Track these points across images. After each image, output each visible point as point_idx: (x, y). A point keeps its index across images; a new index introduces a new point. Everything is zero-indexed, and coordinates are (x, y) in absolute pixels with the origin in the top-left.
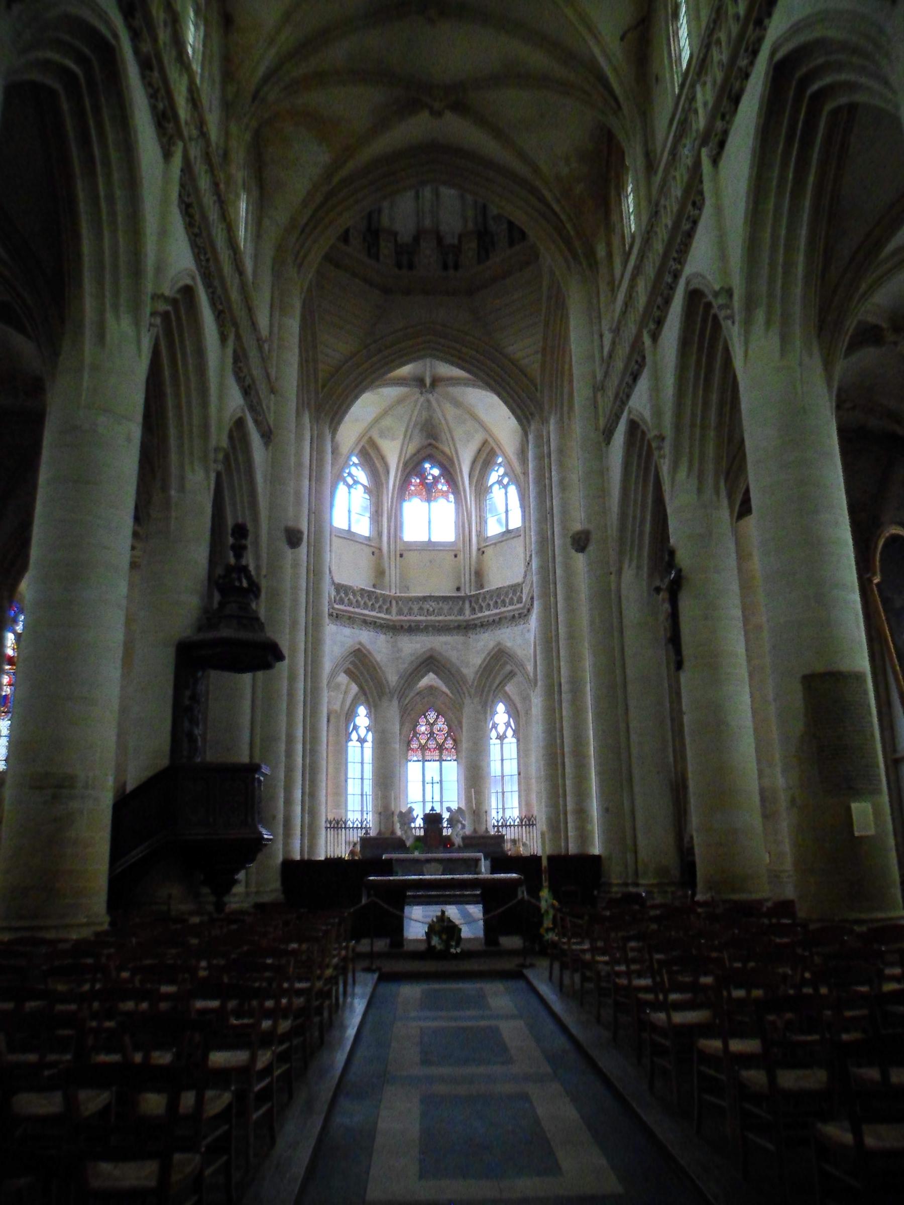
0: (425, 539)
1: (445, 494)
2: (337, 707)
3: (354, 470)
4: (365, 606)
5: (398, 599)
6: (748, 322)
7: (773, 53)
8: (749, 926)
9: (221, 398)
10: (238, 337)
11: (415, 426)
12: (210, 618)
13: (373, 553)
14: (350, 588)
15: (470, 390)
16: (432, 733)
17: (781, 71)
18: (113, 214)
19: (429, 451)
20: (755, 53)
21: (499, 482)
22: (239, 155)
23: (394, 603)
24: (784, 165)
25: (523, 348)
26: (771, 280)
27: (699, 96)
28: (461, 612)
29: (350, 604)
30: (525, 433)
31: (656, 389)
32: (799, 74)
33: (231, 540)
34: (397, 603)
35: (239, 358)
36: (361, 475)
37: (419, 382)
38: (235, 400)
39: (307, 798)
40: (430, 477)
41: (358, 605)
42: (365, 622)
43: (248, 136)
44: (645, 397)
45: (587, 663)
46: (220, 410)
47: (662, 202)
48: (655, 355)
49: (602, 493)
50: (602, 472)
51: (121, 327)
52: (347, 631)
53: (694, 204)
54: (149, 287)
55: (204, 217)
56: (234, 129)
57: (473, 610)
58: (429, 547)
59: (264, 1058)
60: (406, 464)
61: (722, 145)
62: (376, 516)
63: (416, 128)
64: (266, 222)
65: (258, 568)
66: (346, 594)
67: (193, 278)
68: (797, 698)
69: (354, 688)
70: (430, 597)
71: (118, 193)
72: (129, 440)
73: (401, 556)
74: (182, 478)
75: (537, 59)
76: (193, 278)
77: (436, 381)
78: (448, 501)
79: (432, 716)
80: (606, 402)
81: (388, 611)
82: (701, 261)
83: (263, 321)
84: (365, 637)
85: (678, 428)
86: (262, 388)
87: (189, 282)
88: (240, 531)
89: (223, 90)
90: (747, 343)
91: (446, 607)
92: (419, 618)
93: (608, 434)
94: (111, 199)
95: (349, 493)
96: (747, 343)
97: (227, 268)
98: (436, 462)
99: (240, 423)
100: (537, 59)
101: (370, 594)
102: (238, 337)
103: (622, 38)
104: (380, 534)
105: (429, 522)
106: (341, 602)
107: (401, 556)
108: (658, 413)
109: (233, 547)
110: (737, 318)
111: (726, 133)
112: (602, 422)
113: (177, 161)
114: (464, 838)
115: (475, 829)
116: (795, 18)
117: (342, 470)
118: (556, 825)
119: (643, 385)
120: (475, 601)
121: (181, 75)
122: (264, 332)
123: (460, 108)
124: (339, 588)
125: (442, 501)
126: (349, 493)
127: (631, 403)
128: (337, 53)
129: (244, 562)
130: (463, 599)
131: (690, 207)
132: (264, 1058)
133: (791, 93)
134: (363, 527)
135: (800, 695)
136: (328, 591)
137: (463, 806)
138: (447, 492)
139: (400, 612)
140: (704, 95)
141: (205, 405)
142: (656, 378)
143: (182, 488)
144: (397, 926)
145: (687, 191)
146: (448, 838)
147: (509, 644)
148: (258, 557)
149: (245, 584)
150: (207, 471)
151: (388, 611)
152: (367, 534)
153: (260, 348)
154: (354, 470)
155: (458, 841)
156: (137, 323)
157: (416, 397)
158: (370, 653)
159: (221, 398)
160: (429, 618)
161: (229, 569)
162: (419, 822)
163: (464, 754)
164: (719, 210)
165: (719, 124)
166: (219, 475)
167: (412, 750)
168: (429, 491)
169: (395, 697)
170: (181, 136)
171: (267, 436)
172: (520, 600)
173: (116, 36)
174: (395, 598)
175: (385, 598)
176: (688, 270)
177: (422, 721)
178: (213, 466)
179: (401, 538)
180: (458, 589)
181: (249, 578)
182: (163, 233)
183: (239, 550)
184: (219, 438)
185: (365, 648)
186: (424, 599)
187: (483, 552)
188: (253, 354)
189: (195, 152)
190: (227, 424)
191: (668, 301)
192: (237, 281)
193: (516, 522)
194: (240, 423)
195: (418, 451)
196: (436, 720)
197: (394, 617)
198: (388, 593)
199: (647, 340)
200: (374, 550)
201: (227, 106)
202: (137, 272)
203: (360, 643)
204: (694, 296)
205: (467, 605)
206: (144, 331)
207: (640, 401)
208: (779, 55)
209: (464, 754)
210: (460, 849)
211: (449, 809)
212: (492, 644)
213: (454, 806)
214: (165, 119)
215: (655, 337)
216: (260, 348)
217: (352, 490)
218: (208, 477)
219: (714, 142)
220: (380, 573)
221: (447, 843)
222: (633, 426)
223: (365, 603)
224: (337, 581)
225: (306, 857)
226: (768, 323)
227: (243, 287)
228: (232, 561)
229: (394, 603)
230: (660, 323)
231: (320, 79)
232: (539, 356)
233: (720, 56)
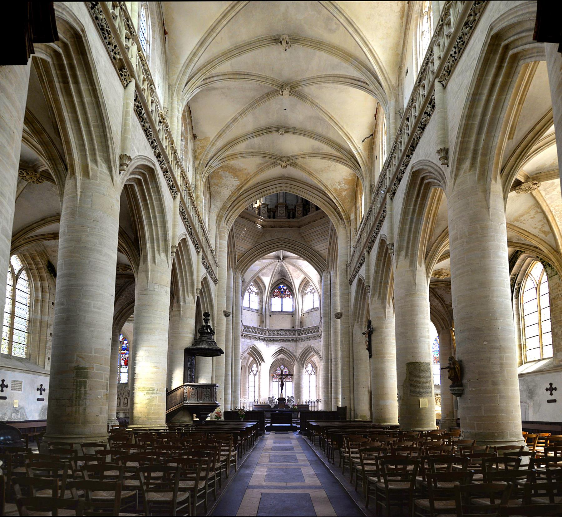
1: (289, 296)
2: (245, 364)
3: (251, 287)
5: (269, 331)
6: (398, 255)
7: (412, 168)
8: (375, 428)
9: (198, 272)
10: (203, 251)
11: (276, 272)
12: (196, 341)
15: (298, 260)
17: (415, 174)
18: (156, 222)
19: (282, 280)
20: (407, 166)
22: (201, 187)
24: (415, 205)
25: (321, 247)
26: (408, 242)
27: (387, 174)
28: (294, 335)
29: (250, 332)
30: (321, 277)
31: (368, 270)
32: (503, 44)
33: (203, 317)
35: (204, 258)
36: (255, 289)
37: (278, 258)
38: (203, 272)
43: (204, 180)
44: (364, 272)
45: (340, 353)
46: (198, 276)
47: (373, 207)
48: (369, 258)
49: (348, 301)
50: (348, 294)
51: (161, 258)
52: (249, 341)
53: (384, 211)
54: (170, 244)
55: (189, 215)
56: (198, 177)
57: (299, 334)
59: (202, 485)
60: (272, 285)
61: (394, 193)
63: (276, 171)
64: (213, 207)
65: (213, 324)
66: (248, 329)
67: (186, 235)
68: (405, 369)
69: (251, 359)
70: (282, 330)
71: (157, 215)
72: (166, 292)
74: (184, 299)
75: (327, 149)
76: (186, 235)
77: (284, 258)
80: (351, 271)
81: (265, 334)
82: (384, 230)
83: (212, 242)
85: (375, 283)
86: (213, 266)
87: (185, 237)
88: (207, 315)
89: (194, 162)
90: (397, 262)
91: (288, 333)
93: (351, 281)
94: (155, 217)
96: (397, 262)
97: (198, 230)
98: (285, 285)
99: (205, 279)
100: (327, 149)
101: (258, 329)
102: (203, 251)
103: (363, 142)
104: (262, 309)
105: (282, 305)
106: (246, 331)
108: (368, 278)
109: (204, 319)
110: (395, 253)
111: (395, 190)
112: (349, 278)
113: (178, 199)
116: (420, 159)
117: (246, 287)
118: (327, 402)
119: (364, 266)
120: (299, 332)
121: (178, 168)
122: (213, 247)
123: (294, 165)
124: (245, 327)
127: (360, 272)
128: (241, 147)
129: (209, 324)
130: (295, 331)
131: (382, 212)
132: (202, 485)
133: (419, 182)
135: (405, 368)
136: (241, 328)
137: (293, 396)
140: (389, 175)
141: (192, 275)
142: (368, 266)
143: (185, 302)
144: (419, 475)
145: (382, 206)
146: (287, 405)
147: (313, 346)
148: (213, 321)
149: (209, 331)
150: (193, 296)
153: (212, 253)
154: (251, 287)
156: (167, 256)
157: (276, 263)
159: (198, 272)
161: (203, 326)
162: (276, 400)
163: (294, 382)
164: (391, 216)
165: (393, 187)
166: (198, 298)
170: (179, 191)
171: (216, 281)
172: (318, 331)
173: (154, 165)
175: (263, 330)
176: (381, 232)
177: (278, 369)
178: (195, 295)
180: (293, 327)
181: (210, 329)
182: (174, 226)
183: (207, 321)
184: (198, 285)
186: (279, 330)
188: (209, 256)
189: (184, 194)
190: (201, 279)
191: (373, 241)
192: (202, 233)
193: (317, 305)
194: (205, 279)
195: (278, 280)
197: (267, 336)
199: (366, 254)
201: (196, 169)
202: (166, 240)
204: (383, 242)
206: (169, 258)
207: (362, 272)
208: (414, 170)
209: (294, 382)
211: (288, 397)
212: (306, 345)
213: (290, 396)
214: (173, 187)
215: (369, 252)
216: (212, 253)
218: (194, 299)
219: (391, 193)
222: (360, 280)
224: (244, 324)
226: (406, 256)
227: (205, 234)
228: (204, 324)
230: (371, 248)
231: (234, 156)
232: (327, 250)
233: (395, 162)
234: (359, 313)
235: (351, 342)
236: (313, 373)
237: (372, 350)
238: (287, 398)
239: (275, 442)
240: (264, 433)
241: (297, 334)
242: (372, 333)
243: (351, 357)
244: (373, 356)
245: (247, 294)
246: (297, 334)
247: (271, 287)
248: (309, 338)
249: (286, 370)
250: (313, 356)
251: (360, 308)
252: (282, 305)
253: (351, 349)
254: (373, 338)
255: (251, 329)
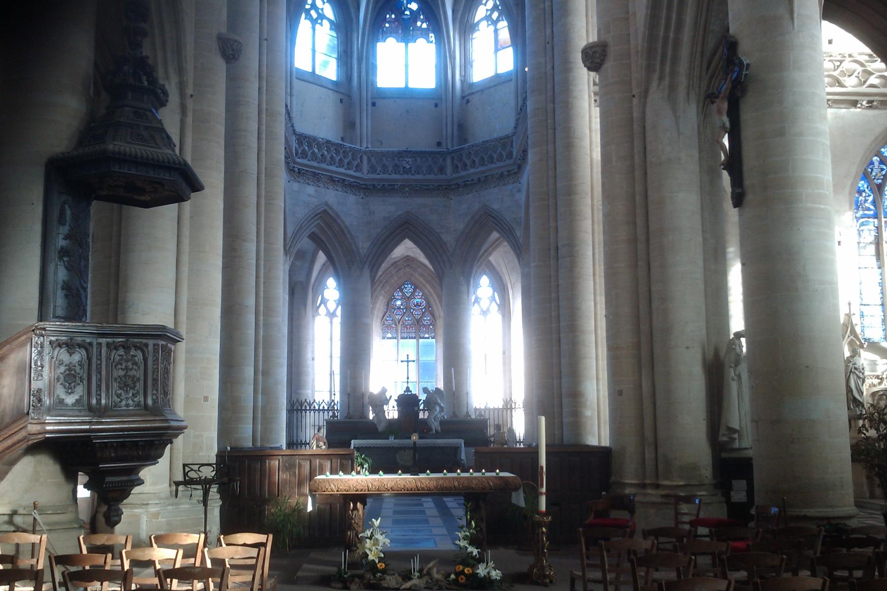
0: (402, 85)
1: (424, 34)
4: (332, 162)
5: (371, 154)
13: (341, 101)
14: (315, 139)
16: (408, 308)
21: (488, 18)
23: (365, 158)
29: (314, 157)
34: (369, 160)
39: (260, 377)
40: (407, 13)
41: (323, 159)
42: (332, 180)
52: (311, 190)
58: (406, 95)
62: (345, 55)
66: (310, 146)
73: (374, 104)
78: (429, 42)
79: (408, 289)
81: (358, 168)
84: (332, 196)
92: (394, 176)
95: (314, 29)
101: (338, 147)
104: (349, 78)
105: (407, 66)
106: (304, 155)
107: (374, 104)
114: (443, 423)
115: (454, 413)
125: (421, 41)
126: (314, 29)
134: (330, 71)
138: (427, 30)
139: (373, 170)
146: (424, 421)
147: (496, 206)
151: (358, 168)
152: (334, 78)
155: (435, 425)
158: (337, 214)
160: (406, 176)
167: (425, 326)
168: (405, 29)
169: (367, 266)
172: (510, 155)
174: (365, 152)
175: (355, 152)
179: (374, 83)
185: (331, 208)
187: (468, 101)
196: (413, 293)
197: (365, 174)
198: (358, 147)
200: (341, 96)
203: (326, 204)
205: (449, 161)
210: (438, 435)
217: (318, 26)
220: (349, 124)
221: (423, 428)
223: (332, 157)
224: (298, 129)
225: (259, 444)
229: (365, 158)
234: (666, 38)
235: (637, 160)
236: (494, 308)
237: (746, 168)
238: (423, 397)
239: (395, 505)
240: (408, 402)
241: (449, 169)
242: (744, 91)
243: (640, 221)
244: (749, 197)
245: (304, 25)
246: (449, 169)
247: (374, 8)
248: (483, 182)
249: (417, 300)
250: (495, 245)
251: (668, 19)
252: (407, 66)
253: (639, 188)
254: (747, 115)
255: (319, 146)
